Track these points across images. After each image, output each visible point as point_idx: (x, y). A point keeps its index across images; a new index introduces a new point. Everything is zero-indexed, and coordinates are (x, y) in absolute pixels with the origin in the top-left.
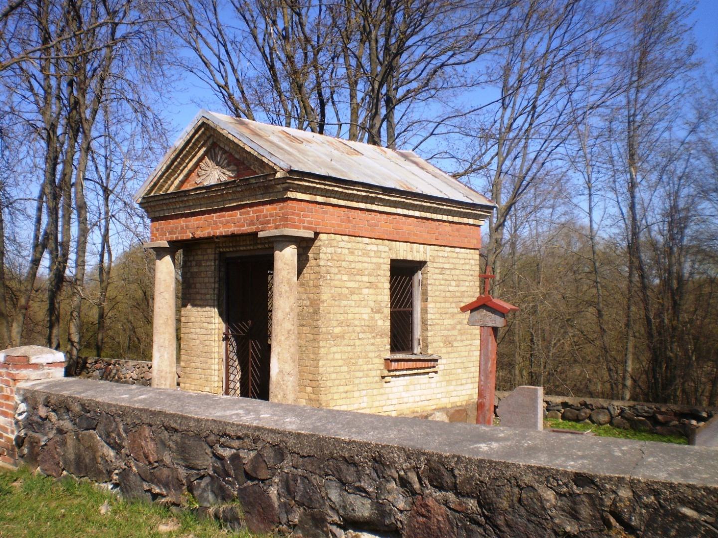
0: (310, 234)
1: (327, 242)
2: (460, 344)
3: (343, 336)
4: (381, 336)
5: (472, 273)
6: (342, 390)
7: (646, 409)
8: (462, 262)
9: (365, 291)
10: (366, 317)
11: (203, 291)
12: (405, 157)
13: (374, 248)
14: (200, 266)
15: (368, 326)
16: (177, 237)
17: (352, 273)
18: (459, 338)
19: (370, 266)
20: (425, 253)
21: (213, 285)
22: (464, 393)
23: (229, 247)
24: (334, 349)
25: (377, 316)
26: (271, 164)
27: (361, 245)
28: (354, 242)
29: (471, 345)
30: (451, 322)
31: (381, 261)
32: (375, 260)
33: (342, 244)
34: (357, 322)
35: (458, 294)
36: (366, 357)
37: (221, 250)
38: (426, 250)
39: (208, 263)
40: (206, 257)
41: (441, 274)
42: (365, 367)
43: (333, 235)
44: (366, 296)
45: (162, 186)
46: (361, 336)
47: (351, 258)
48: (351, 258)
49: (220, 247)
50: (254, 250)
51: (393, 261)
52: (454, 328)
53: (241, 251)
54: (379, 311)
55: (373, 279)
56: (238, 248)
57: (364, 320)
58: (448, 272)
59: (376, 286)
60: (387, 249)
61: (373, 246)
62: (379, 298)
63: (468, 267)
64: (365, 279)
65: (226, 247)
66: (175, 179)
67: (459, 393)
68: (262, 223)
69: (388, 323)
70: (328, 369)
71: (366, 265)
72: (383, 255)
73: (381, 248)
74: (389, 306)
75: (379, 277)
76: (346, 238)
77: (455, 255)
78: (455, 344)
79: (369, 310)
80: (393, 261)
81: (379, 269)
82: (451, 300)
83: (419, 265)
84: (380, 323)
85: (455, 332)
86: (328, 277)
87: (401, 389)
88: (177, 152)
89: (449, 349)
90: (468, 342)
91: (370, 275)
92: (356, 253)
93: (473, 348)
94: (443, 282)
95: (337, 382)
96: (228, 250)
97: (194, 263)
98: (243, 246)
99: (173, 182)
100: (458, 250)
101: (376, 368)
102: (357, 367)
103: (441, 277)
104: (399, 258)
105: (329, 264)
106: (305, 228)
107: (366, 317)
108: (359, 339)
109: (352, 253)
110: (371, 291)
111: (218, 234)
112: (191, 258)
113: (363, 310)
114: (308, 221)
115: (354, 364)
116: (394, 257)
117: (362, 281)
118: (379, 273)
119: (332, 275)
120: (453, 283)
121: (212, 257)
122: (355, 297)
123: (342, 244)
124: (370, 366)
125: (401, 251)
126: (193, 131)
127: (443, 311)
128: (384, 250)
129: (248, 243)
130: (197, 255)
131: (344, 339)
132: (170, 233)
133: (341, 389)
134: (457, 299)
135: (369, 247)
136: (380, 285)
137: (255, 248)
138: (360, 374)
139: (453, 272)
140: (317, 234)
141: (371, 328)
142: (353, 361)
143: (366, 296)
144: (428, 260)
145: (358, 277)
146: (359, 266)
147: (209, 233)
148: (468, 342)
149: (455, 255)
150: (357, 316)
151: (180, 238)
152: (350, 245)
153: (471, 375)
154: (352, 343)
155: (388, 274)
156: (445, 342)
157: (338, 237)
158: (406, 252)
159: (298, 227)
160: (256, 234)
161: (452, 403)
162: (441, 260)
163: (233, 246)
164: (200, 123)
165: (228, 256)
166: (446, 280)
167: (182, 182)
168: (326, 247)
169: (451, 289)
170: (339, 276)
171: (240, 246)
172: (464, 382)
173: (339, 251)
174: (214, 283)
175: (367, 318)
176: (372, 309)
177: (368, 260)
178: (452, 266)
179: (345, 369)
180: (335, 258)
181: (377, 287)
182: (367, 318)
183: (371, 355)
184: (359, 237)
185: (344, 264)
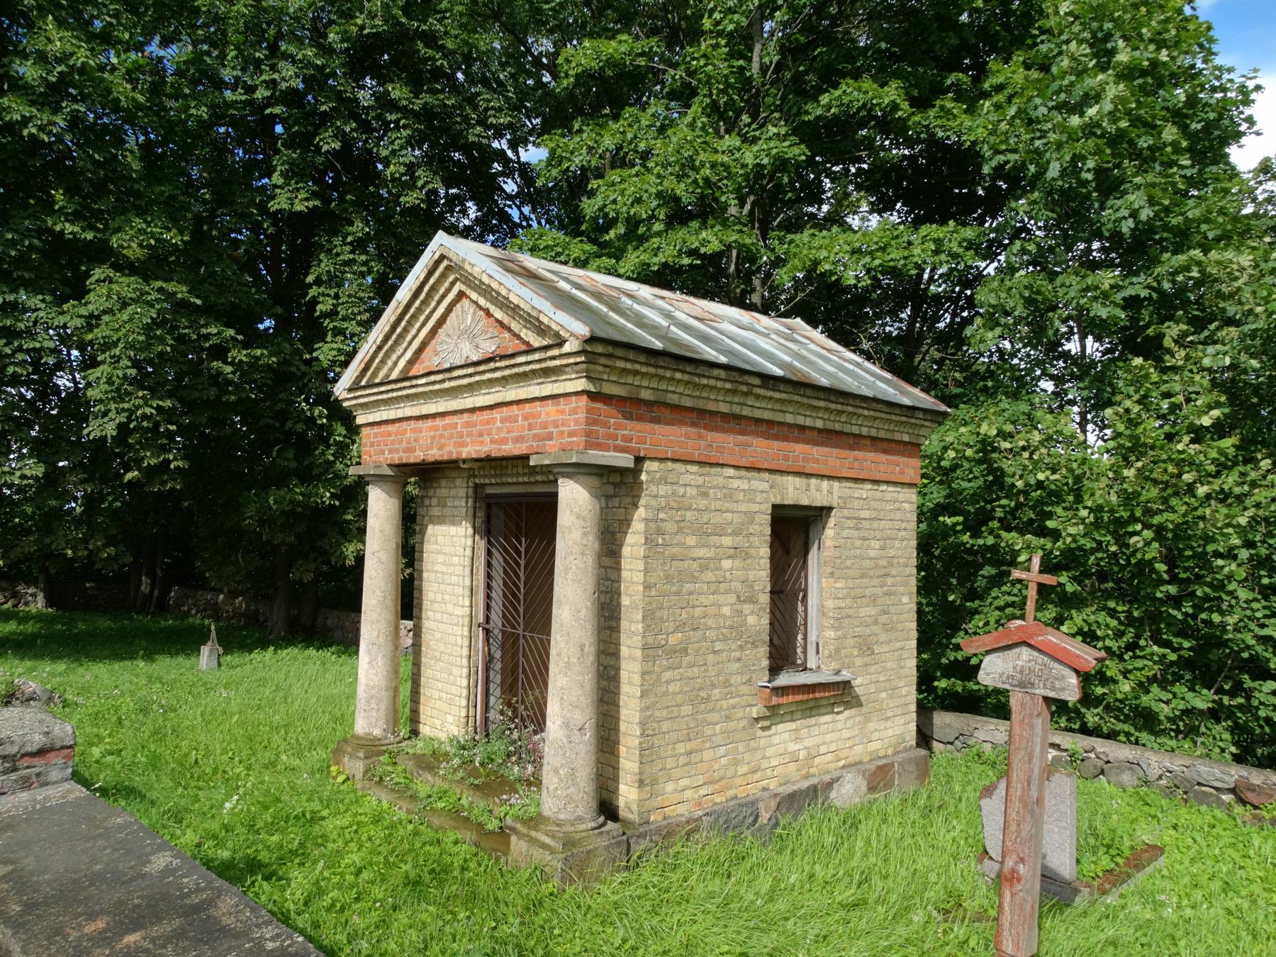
0: (626, 460)
1: (658, 476)
2: (885, 648)
3: (686, 649)
4: (753, 644)
5: (904, 525)
6: (682, 751)
7: (1219, 775)
8: (889, 507)
9: (727, 564)
10: (726, 610)
11: (447, 550)
12: (397, 628)
13: (743, 485)
14: (445, 506)
15: (731, 627)
16: (400, 458)
17: (702, 533)
18: (883, 638)
19: (737, 518)
20: (831, 493)
21: (463, 540)
22: (890, 732)
23: (491, 476)
24: (667, 675)
25: (747, 608)
26: (554, 326)
27: (721, 479)
28: (708, 474)
29: (902, 649)
30: (872, 611)
31: (755, 508)
32: (743, 508)
33: (687, 478)
34: (710, 622)
35: (883, 563)
36: (727, 684)
37: (477, 481)
38: (831, 487)
39: (457, 503)
40: (453, 492)
41: (857, 529)
42: (724, 704)
43: (670, 463)
44: (728, 574)
45: (378, 370)
46: (718, 646)
47: (702, 503)
48: (702, 503)
49: (475, 476)
50: (530, 483)
51: (775, 507)
52: (876, 622)
53: (509, 484)
54: (752, 600)
55: (739, 540)
56: (504, 480)
57: (724, 616)
58: (866, 524)
59: (747, 553)
60: (765, 486)
61: (740, 483)
62: (752, 575)
63: (898, 516)
64: (727, 541)
65: (485, 476)
66: (400, 357)
67: (882, 735)
68: (537, 438)
69: (765, 621)
70: (657, 714)
71: (729, 515)
72: (759, 498)
73: (757, 484)
74: (769, 588)
75: (751, 539)
76: (694, 468)
77: (879, 495)
78: (877, 649)
79: (732, 599)
80: (775, 507)
81: (752, 522)
82: (872, 573)
83: (819, 515)
84: (751, 620)
85: (876, 629)
86: (660, 541)
87: (786, 736)
88: (399, 311)
89: (867, 659)
90: (898, 645)
91: (734, 534)
92: (712, 495)
93: (755, 540)
94: (858, 543)
95: (673, 736)
96: (487, 481)
97: (434, 501)
98: (512, 475)
99: (396, 363)
100: (883, 487)
101: (743, 703)
102: (711, 705)
103: (856, 533)
104: (786, 502)
105: (662, 516)
106: (618, 449)
107: (726, 610)
108: (715, 652)
109: (705, 495)
110: (738, 563)
111: (464, 456)
112: (431, 493)
113: (721, 598)
114: (623, 436)
115: (707, 700)
116: (778, 501)
117: (721, 546)
118: (751, 531)
119: (667, 537)
120: (877, 544)
121: (462, 492)
122: (709, 576)
123: (687, 478)
124: (732, 701)
125: (791, 489)
126: (426, 271)
127: (858, 592)
128: (761, 488)
129: (520, 471)
130: (440, 487)
131: (687, 655)
132: (390, 451)
133: (681, 748)
134: (881, 572)
135: (736, 484)
136: (752, 551)
137: (532, 479)
138: (714, 717)
139: (875, 524)
140: (639, 460)
141: (738, 629)
142: (703, 694)
143: (728, 574)
144: (835, 505)
145: (714, 539)
146: (717, 519)
147: (450, 452)
148: (898, 645)
149: (879, 495)
150: (712, 610)
151: (404, 461)
152: (700, 480)
153: (902, 701)
154: (700, 660)
155: (768, 531)
156: (860, 647)
157: (680, 467)
158: (795, 492)
159: (605, 448)
160: (526, 458)
161: (872, 752)
162: (856, 504)
163: (496, 475)
164: (436, 256)
165: (490, 491)
166: (865, 539)
167: (411, 362)
168: (658, 482)
169: (872, 553)
170: (679, 538)
171: (509, 476)
172: (890, 714)
173: (681, 491)
174: (466, 536)
175: (728, 614)
176: (738, 597)
177: (735, 507)
178: (874, 514)
179: (687, 709)
180: (673, 504)
181: (748, 556)
182: (728, 614)
183: (736, 680)
184: (717, 465)
185: (689, 515)
